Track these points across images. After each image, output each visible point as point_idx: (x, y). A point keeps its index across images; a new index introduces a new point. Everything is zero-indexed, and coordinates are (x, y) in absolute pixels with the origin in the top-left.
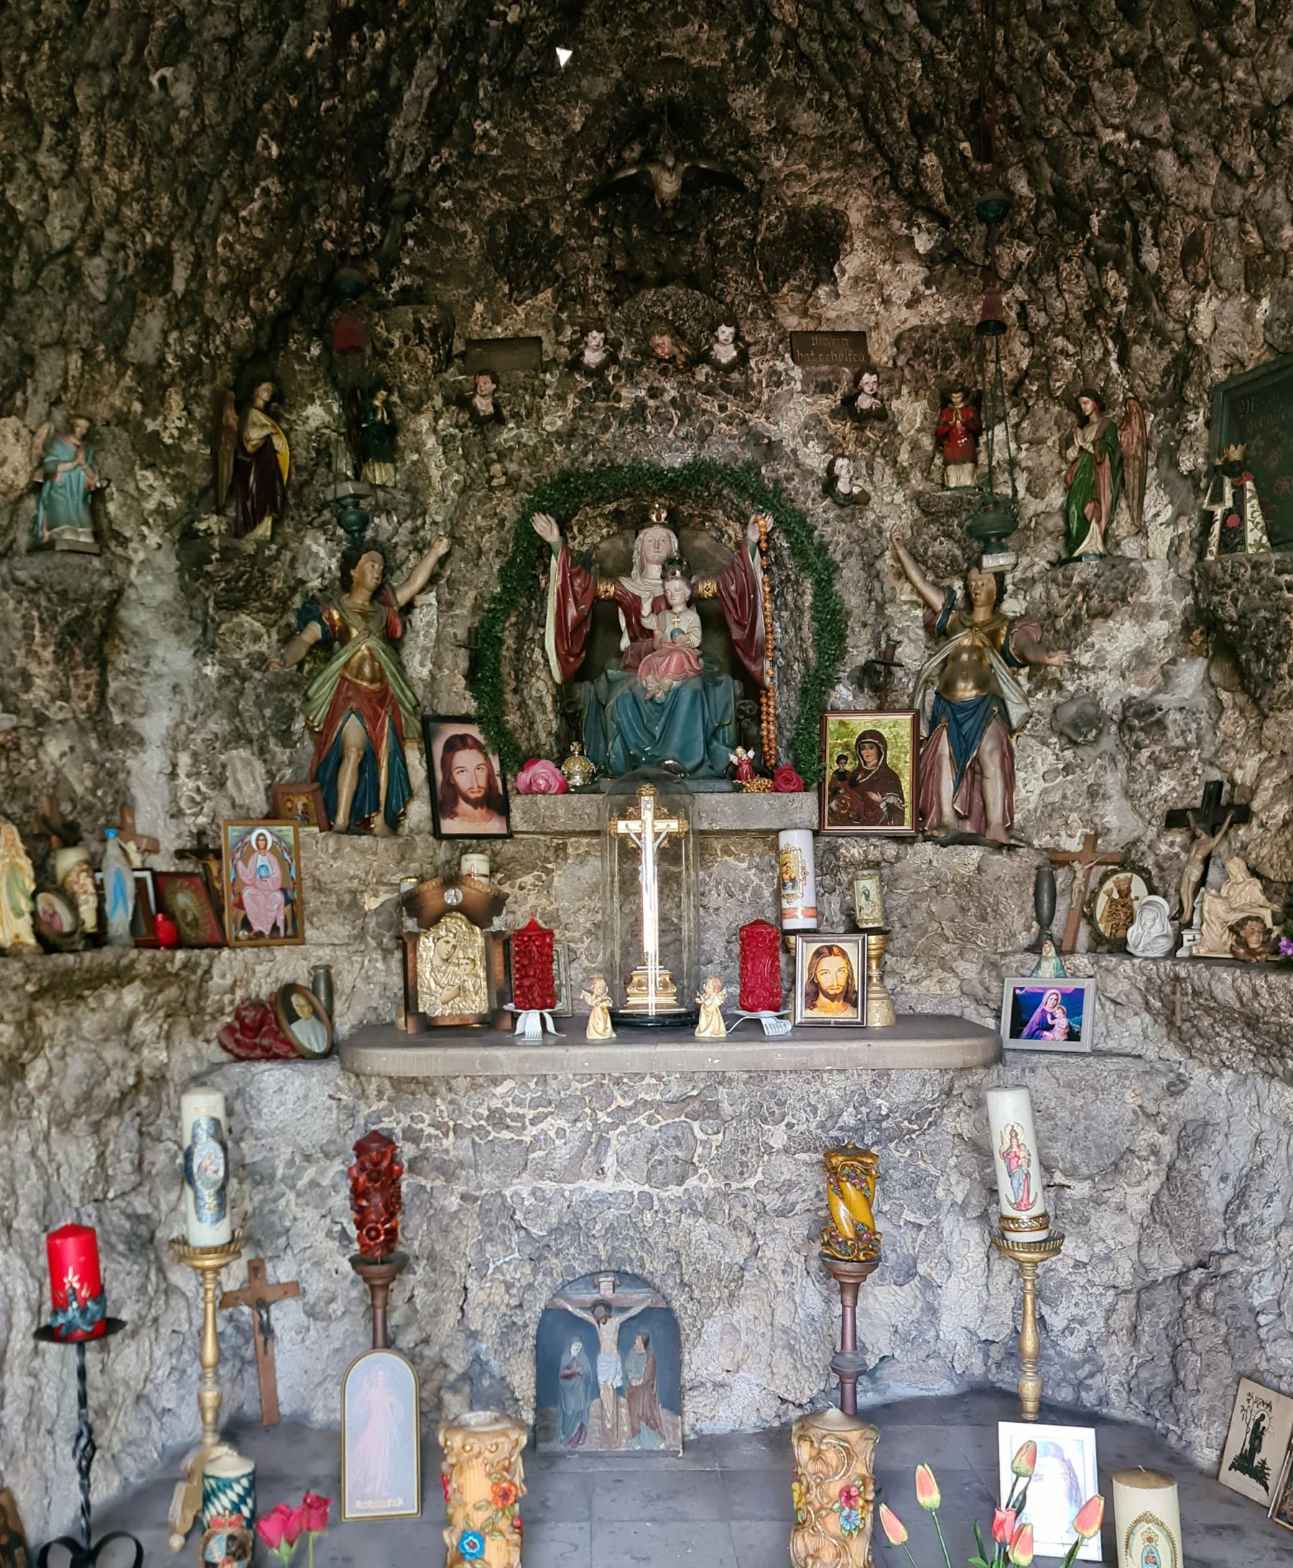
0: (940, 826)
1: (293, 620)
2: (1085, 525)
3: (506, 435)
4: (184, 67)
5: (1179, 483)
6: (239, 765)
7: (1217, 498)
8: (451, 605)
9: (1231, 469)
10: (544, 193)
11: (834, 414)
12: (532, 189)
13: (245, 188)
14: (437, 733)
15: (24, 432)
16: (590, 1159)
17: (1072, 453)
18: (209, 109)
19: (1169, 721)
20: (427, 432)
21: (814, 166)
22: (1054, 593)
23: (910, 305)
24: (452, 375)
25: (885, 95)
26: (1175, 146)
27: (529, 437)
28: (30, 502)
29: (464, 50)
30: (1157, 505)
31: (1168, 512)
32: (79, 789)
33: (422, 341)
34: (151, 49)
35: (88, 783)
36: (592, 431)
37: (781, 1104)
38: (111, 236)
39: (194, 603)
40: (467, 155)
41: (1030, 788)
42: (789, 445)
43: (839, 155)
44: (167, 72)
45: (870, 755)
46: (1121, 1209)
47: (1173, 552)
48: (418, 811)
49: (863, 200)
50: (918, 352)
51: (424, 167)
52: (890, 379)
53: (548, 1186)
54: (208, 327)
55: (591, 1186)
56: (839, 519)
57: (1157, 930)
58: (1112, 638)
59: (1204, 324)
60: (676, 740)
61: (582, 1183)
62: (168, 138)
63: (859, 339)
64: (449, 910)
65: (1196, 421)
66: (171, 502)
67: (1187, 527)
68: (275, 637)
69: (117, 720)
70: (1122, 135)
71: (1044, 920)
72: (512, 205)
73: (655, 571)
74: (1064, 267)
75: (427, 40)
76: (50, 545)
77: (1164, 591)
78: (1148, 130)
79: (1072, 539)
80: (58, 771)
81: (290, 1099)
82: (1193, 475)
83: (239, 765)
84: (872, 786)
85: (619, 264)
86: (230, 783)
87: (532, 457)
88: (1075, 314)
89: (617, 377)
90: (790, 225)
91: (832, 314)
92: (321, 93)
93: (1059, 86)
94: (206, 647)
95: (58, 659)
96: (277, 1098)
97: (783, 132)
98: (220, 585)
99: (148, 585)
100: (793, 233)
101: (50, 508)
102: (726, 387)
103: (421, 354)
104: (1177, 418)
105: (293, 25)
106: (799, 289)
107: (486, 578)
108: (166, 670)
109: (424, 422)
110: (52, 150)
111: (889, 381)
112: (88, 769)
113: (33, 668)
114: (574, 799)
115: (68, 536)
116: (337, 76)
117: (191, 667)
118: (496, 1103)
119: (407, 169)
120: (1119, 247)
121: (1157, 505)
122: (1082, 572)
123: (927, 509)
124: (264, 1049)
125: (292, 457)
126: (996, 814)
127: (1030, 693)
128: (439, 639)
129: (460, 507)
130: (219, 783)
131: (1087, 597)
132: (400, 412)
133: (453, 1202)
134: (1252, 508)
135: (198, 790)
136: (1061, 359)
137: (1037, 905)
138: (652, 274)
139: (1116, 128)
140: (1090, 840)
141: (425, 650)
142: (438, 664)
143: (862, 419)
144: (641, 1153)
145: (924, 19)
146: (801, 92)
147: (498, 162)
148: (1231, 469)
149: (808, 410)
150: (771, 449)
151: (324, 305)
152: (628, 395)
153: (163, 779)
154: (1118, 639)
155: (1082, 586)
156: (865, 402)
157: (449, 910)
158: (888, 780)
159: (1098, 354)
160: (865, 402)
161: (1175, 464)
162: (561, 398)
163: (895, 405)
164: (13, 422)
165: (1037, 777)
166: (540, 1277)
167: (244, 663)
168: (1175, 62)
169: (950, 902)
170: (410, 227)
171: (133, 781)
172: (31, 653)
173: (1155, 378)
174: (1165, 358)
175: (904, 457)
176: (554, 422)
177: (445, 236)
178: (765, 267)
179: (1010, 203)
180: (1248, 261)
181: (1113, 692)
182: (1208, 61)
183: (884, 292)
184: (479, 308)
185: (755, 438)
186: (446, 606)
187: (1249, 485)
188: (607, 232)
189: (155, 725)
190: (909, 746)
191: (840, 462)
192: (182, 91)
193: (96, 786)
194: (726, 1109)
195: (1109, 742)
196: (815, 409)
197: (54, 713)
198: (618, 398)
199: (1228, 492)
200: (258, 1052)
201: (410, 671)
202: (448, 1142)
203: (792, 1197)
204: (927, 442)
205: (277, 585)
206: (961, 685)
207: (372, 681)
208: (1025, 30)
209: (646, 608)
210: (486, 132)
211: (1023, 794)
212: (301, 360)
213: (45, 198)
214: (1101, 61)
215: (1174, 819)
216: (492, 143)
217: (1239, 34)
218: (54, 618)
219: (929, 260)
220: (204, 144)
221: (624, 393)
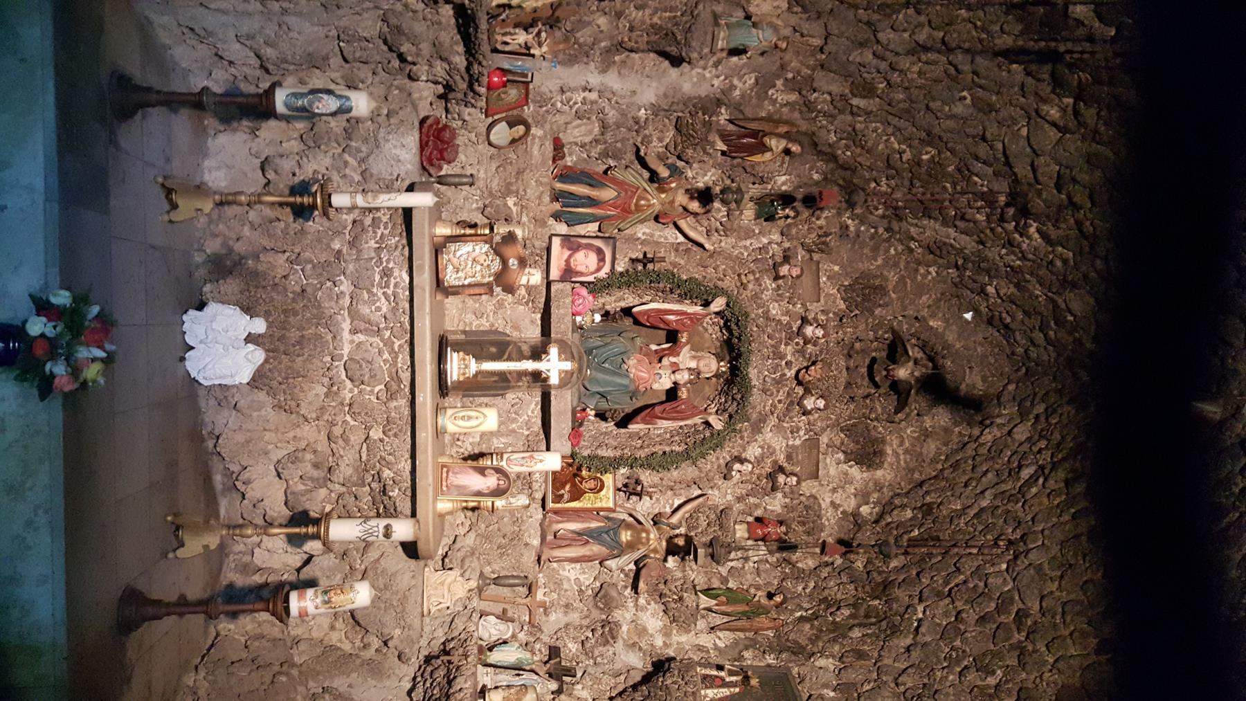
0: (551, 522)
1: (670, 161)
2: (715, 597)
3: (768, 283)
4: (971, 110)
5: (737, 650)
6: (589, 127)
7: (731, 673)
8: (677, 250)
9: (746, 678)
10: (897, 305)
11: (775, 462)
12: (899, 298)
13: (907, 140)
14: (607, 244)
15: (779, 11)
16: (363, 326)
17: (752, 591)
18: (948, 122)
19: (608, 647)
20: (772, 239)
21: (907, 452)
22: (678, 583)
23: (832, 503)
24: (801, 254)
25: (943, 490)
26: (914, 644)
27: (767, 295)
28: (741, 14)
29: (973, 262)
30: (724, 639)
31: (721, 644)
32: (578, 35)
33: (819, 236)
34: (980, 92)
35: (582, 40)
36: (769, 330)
37: (395, 435)
38: (883, 66)
39: (681, 105)
40: (919, 263)
41: (571, 572)
42: (759, 438)
43: (912, 465)
44: (968, 101)
45: (591, 484)
46: (332, 628)
47: (700, 648)
48: (562, 228)
49: (889, 478)
50: (807, 508)
51: (913, 239)
52: (793, 492)
53: (346, 301)
54: (831, 117)
55: (346, 326)
56: (719, 466)
57: (494, 632)
58: (653, 615)
59: (822, 662)
60: (600, 376)
61: (348, 321)
62: (934, 99)
63: (815, 476)
64: (504, 262)
65: (770, 659)
66: (737, 92)
67: (714, 658)
68: (660, 150)
69: (617, 58)
70: (920, 616)
71: (497, 581)
72: (890, 287)
73: (693, 365)
74: (852, 586)
75: (982, 243)
76: (717, 24)
77: (678, 643)
78: (922, 630)
79: (707, 592)
80: (589, 23)
81: (397, 151)
82: (740, 658)
83: (589, 127)
84: (574, 485)
85: (857, 345)
86: (579, 121)
87: (756, 296)
88: (826, 592)
89: (797, 344)
90: (876, 439)
91: (828, 461)
92: (954, 185)
93: (946, 583)
94: (656, 110)
95: (652, 26)
96: (398, 144)
97: (926, 434)
98: (690, 123)
99: (691, 77)
100: (874, 441)
101: (739, 25)
102: (792, 403)
103: (813, 236)
104: (771, 649)
105: (990, 170)
106: (842, 443)
107: (689, 269)
108: (644, 86)
109: (776, 237)
110: (930, 36)
111: (792, 492)
112: (590, 40)
113: (648, 12)
114: (569, 318)
115: (722, 34)
116: (963, 193)
117: (645, 101)
118: (396, 273)
119: (912, 229)
120: (865, 618)
121: (724, 639)
122: (689, 598)
123: (723, 513)
124: (427, 143)
125: (759, 163)
126: (559, 553)
127: (622, 570)
128: (658, 243)
129: (730, 257)
130: (578, 116)
131: (675, 601)
132: (781, 223)
133: (336, 245)
134: (725, 692)
135: (576, 103)
136: (803, 585)
137: (506, 577)
138: (852, 364)
139: (924, 612)
140: (543, 605)
141: (652, 236)
142: (643, 243)
143: (771, 477)
144: (366, 355)
145: (982, 510)
146: (946, 444)
147: (914, 280)
148: (746, 678)
149: (778, 448)
150: (757, 429)
151: (841, 182)
152: (788, 351)
153: (584, 83)
154: (653, 619)
155: (681, 599)
156: (781, 479)
157: (504, 262)
158: (577, 495)
159: (806, 605)
160: (781, 479)
161: (747, 648)
162: (787, 313)
163: (779, 495)
164: (785, 5)
165: (576, 576)
166: (291, 296)
167: (647, 132)
168: (958, 643)
169: (509, 529)
170: (881, 230)
171: (583, 66)
172: (656, 11)
173: (792, 636)
174: (803, 641)
175: (752, 500)
176: (775, 310)
177: (875, 249)
178: (854, 425)
179: (887, 557)
180: (854, 684)
181: (624, 616)
182: (958, 661)
183: (839, 489)
184: (836, 268)
185: (763, 419)
186: (676, 248)
187: (737, 690)
188: (876, 339)
189: (613, 80)
190: (597, 505)
191: (750, 466)
192: (959, 109)
193: (580, 45)
194: (393, 404)
195: (596, 614)
196: (778, 452)
197: (624, 24)
198: (787, 344)
199: (734, 679)
200: (425, 139)
201: (640, 226)
202: (372, 244)
203: (340, 442)
204: (759, 513)
205: (690, 152)
206: (629, 533)
207: (637, 205)
208: (976, 564)
209: (673, 359)
210: (929, 273)
211: (567, 567)
212: (811, 169)
213: (905, 31)
214: (960, 605)
215: (554, 652)
216: (924, 276)
217: (972, 677)
218: (676, 24)
219: (856, 514)
220: (930, 118)
221: (789, 348)
